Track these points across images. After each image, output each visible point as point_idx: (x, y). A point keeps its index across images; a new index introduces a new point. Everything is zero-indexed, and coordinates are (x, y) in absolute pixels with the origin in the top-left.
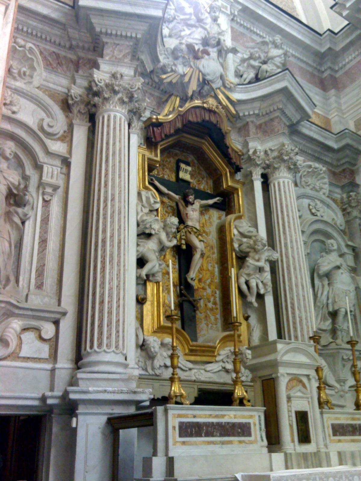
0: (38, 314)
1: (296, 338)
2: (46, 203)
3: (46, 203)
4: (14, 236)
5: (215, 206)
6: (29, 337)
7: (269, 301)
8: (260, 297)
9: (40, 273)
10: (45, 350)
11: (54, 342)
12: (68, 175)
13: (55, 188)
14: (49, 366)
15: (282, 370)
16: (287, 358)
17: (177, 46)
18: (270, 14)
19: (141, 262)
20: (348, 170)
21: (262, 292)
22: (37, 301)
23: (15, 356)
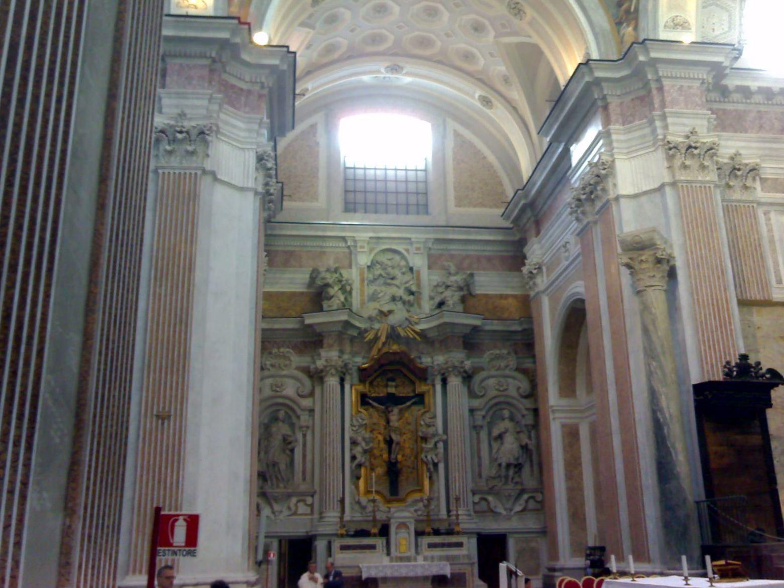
0: (303, 494)
1: (333, 508)
2: (304, 436)
3: (304, 436)
4: (288, 460)
5: (415, 403)
6: (301, 505)
7: (441, 466)
8: (436, 465)
9: (304, 473)
10: (308, 510)
11: (312, 506)
12: (314, 419)
13: (308, 427)
14: (310, 517)
15: (392, 521)
16: (396, 515)
17: (264, 330)
18: (540, 175)
19: (353, 458)
20: (333, 371)
21: (436, 461)
22: (303, 487)
23: (295, 513)
